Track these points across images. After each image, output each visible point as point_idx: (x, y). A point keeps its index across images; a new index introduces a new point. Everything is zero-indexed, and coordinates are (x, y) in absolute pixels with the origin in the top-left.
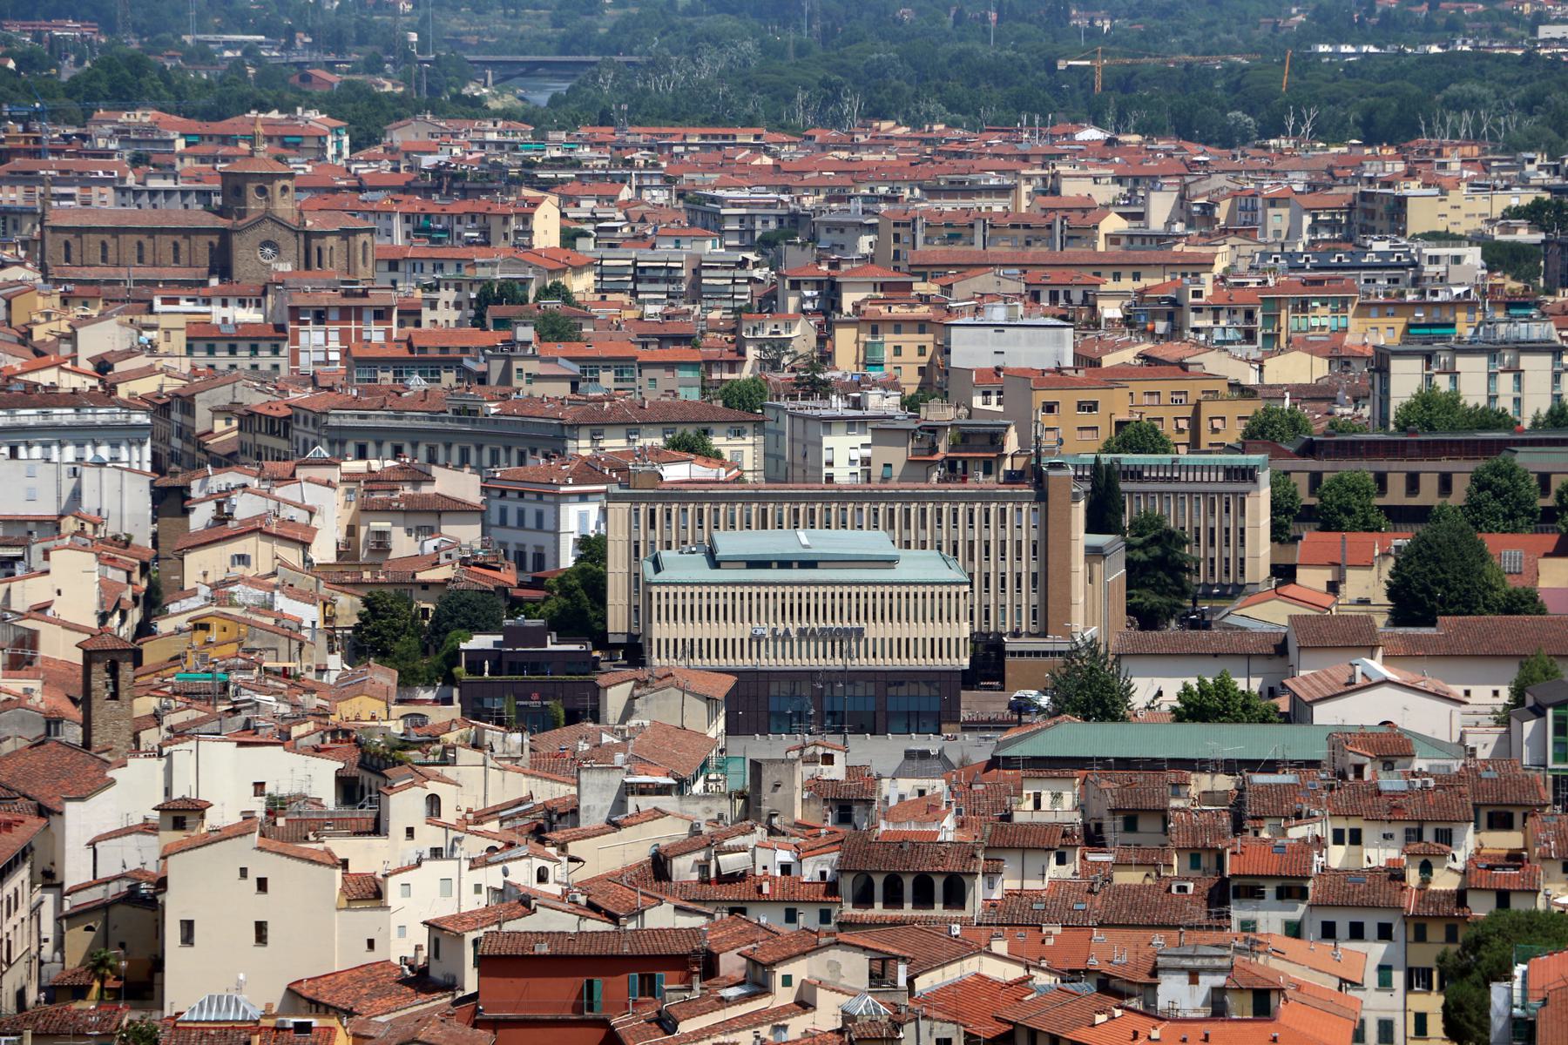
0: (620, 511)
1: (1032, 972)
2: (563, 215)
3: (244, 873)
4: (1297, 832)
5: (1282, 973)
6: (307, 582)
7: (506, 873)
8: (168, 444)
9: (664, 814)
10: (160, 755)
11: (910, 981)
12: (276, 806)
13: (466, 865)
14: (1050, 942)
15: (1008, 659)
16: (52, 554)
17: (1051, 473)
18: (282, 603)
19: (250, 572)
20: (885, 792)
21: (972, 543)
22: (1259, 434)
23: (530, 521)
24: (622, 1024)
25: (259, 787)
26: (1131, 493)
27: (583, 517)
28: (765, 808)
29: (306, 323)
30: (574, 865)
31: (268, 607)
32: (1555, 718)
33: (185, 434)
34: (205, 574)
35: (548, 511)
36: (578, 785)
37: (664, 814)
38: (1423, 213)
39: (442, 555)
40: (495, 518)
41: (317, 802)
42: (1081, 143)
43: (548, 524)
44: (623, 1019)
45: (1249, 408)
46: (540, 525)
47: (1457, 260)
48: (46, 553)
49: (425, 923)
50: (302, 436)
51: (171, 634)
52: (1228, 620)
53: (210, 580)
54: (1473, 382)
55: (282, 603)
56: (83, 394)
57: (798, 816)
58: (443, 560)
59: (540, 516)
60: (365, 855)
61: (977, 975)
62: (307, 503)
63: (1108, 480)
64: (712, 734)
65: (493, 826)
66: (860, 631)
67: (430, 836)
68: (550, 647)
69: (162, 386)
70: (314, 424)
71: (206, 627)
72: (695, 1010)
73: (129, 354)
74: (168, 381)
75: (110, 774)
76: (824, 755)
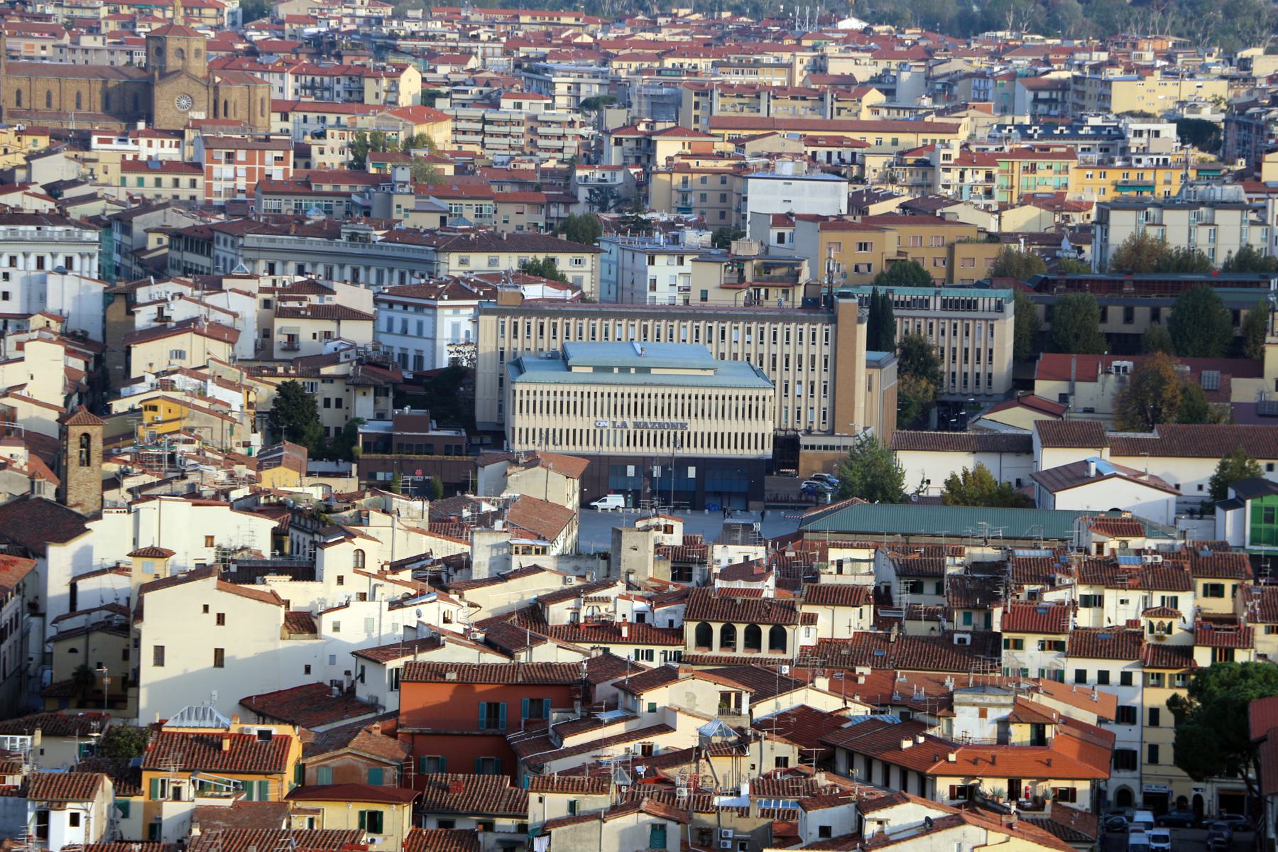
0: (488, 322)
1: (849, 704)
2: (424, 80)
3: (206, 608)
4: (1050, 597)
5: (1054, 711)
6: (233, 374)
7: (419, 614)
8: (110, 259)
9: (541, 570)
10: (129, 512)
11: (750, 711)
12: (225, 555)
13: (386, 605)
14: (862, 680)
15: (802, 451)
16: (27, 345)
17: (841, 301)
18: (213, 390)
19: (186, 364)
20: (716, 557)
21: (800, 357)
22: (1003, 272)
23: (412, 330)
24: (516, 739)
25: (209, 540)
26: (902, 318)
27: (456, 327)
28: (624, 568)
29: (219, 162)
30: (474, 610)
31: (202, 394)
32: (1253, 508)
33: (123, 251)
34: (151, 365)
35: (427, 321)
36: (471, 544)
37: (541, 570)
38: (1126, 95)
39: (342, 354)
40: (383, 326)
41: (258, 553)
42: (844, 31)
43: (427, 332)
44: (517, 734)
45: (993, 250)
46: (420, 333)
47: (1157, 133)
48: (20, 346)
49: (353, 653)
50: (222, 255)
51: (125, 413)
52: (980, 423)
53: (156, 369)
54: (1177, 231)
55: (213, 390)
56: (43, 215)
57: (650, 574)
58: (342, 359)
59: (420, 325)
60: (299, 594)
61: (803, 706)
62: (232, 309)
63: (883, 308)
64: (569, 506)
65: (406, 575)
66: (684, 426)
67: (357, 583)
68: (432, 433)
69: (104, 210)
70: (232, 246)
71: (154, 408)
72: (576, 728)
73: (74, 183)
74: (109, 206)
75: (88, 526)
76: (666, 527)
